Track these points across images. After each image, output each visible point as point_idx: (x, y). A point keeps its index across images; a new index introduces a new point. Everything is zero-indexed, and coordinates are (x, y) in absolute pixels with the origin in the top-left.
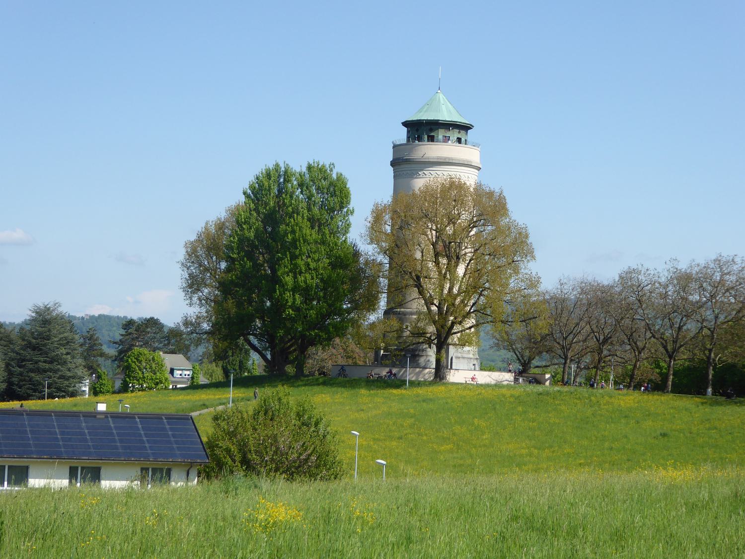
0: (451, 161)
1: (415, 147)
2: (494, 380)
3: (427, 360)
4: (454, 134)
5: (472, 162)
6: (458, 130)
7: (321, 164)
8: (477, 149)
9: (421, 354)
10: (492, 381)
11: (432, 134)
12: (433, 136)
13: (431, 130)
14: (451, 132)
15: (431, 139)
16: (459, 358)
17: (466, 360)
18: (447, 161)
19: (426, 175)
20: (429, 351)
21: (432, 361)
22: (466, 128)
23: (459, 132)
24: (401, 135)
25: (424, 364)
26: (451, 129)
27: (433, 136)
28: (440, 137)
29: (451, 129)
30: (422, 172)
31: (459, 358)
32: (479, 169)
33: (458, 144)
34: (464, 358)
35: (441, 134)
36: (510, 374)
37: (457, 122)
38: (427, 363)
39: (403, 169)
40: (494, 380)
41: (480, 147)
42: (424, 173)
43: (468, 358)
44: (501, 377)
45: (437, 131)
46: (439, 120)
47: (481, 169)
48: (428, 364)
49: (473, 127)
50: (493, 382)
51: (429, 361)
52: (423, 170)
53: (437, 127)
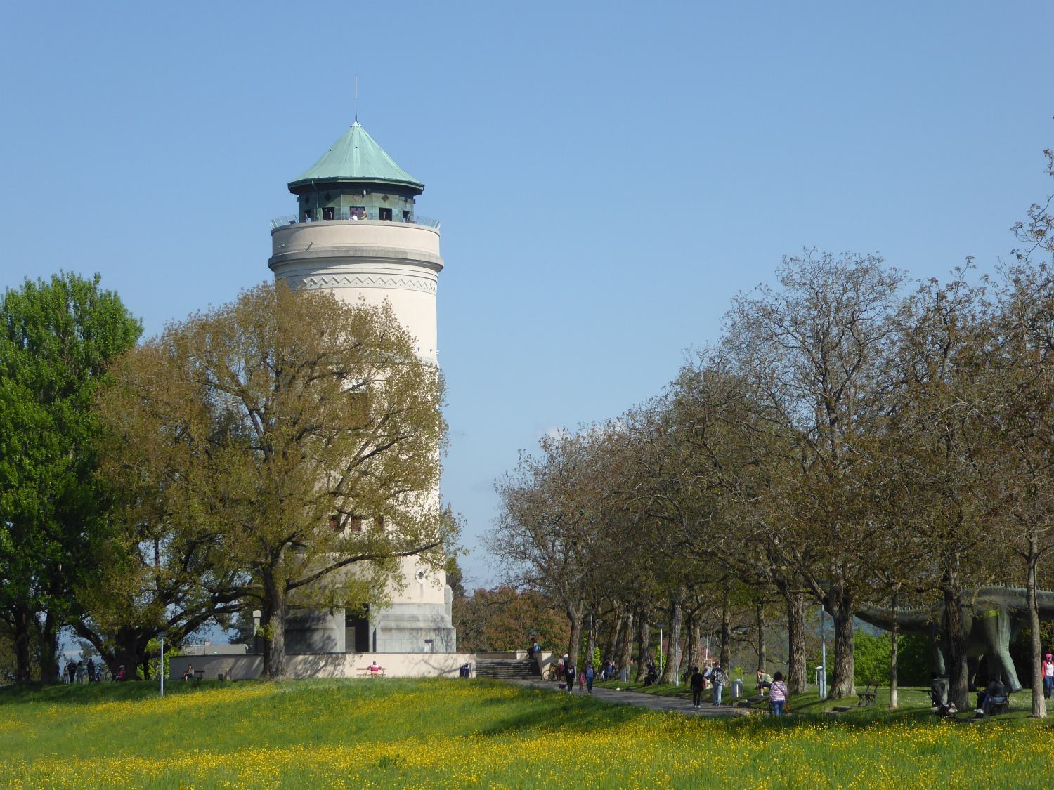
0: (365, 255)
1: (295, 232)
2: (435, 668)
3: (325, 637)
4: (375, 203)
5: (406, 253)
6: (382, 195)
7: (77, 276)
8: (434, 229)
9: (314, 627)
10: (431, 670)
11: (330, 205)
12: (332, 210)
13: (329, 198)
14: (366, 199)
15: (329, 214)
16: (390, 630)
17: (407, 635)
18: (351, 254)
19: (315, 283)
20: (330, 621)
21: (334, 640)
22: (408, 191)
23: (385, 199)
24: (291, 206)
25: (321, 645)
26: (365, 192)
27: (332, 210)
28: (345, 210)
29: (365, 192)
30: (309, 279)
31: (390, 630)
32: (438, 268)
33: (405, 224)
34: (400, 629)
35: (345, 203)
36: (468, 655)
37: (374, 179)
38: (327, 642)
39: (292, 274)
40: (435, 668)
41: (439, 227)
42: (312, 280)
43: (413, 629)
44: (450, 662)
45: (338, 199)
46: (337, 178)
47: (442, 267)
48: (328, 644)
49: (423, 186)
50: (434, 674)
51: (329, 638)
52: (310, 275)
53: (339, 190)
